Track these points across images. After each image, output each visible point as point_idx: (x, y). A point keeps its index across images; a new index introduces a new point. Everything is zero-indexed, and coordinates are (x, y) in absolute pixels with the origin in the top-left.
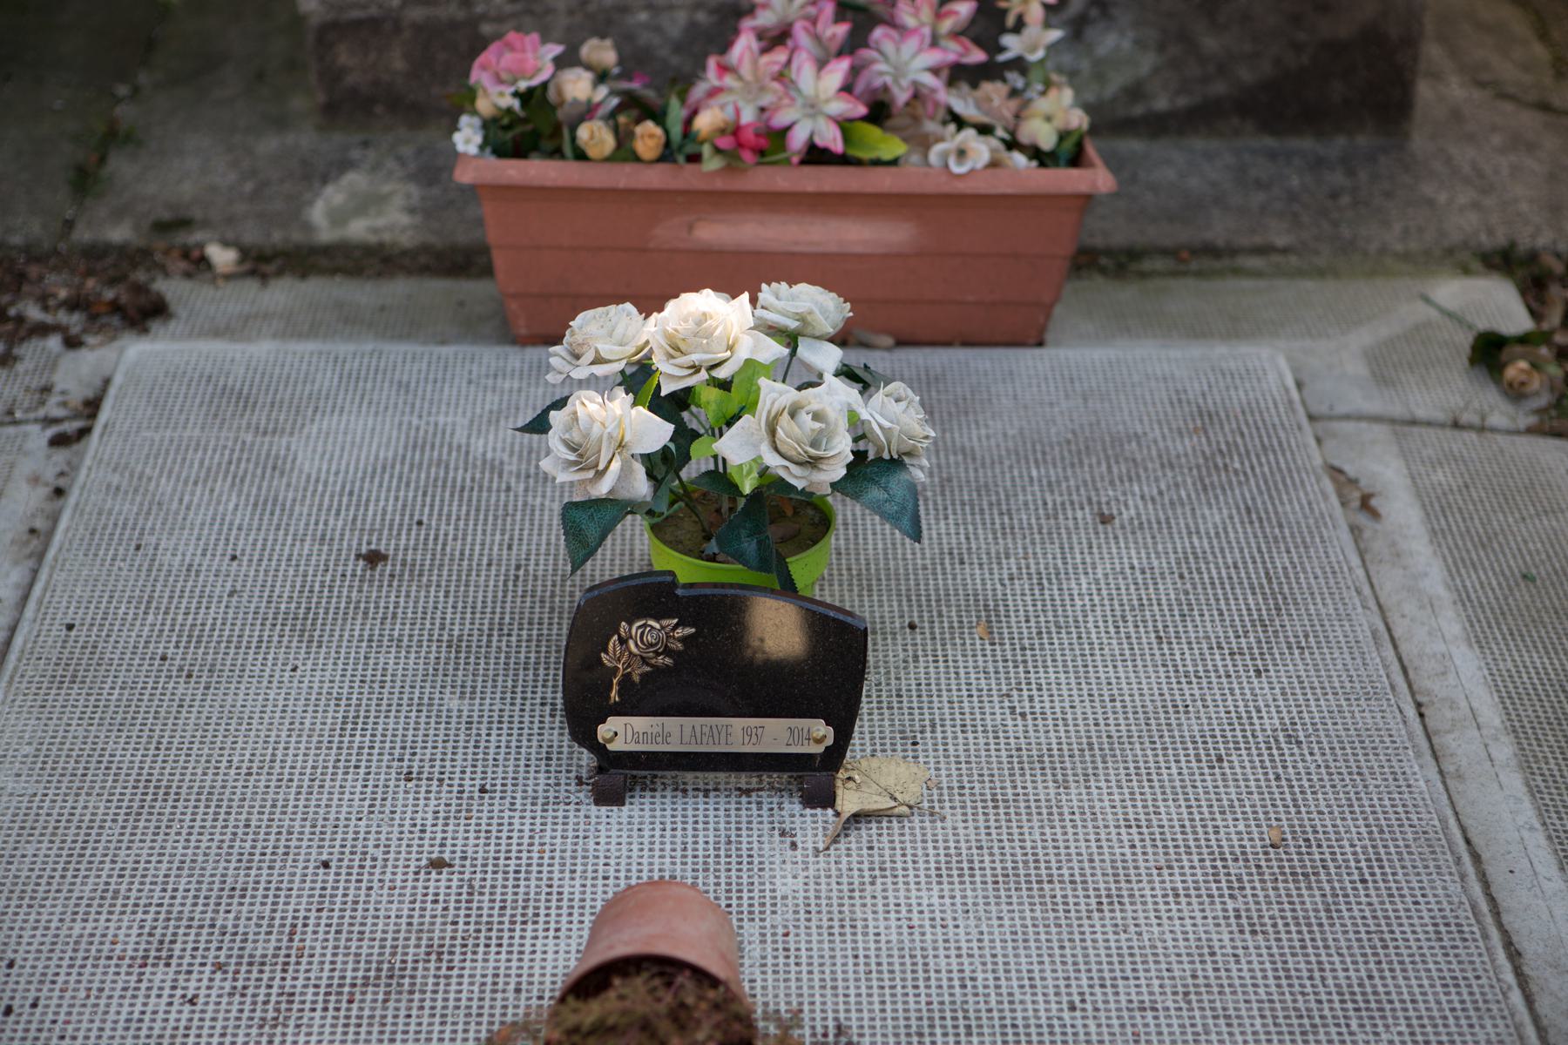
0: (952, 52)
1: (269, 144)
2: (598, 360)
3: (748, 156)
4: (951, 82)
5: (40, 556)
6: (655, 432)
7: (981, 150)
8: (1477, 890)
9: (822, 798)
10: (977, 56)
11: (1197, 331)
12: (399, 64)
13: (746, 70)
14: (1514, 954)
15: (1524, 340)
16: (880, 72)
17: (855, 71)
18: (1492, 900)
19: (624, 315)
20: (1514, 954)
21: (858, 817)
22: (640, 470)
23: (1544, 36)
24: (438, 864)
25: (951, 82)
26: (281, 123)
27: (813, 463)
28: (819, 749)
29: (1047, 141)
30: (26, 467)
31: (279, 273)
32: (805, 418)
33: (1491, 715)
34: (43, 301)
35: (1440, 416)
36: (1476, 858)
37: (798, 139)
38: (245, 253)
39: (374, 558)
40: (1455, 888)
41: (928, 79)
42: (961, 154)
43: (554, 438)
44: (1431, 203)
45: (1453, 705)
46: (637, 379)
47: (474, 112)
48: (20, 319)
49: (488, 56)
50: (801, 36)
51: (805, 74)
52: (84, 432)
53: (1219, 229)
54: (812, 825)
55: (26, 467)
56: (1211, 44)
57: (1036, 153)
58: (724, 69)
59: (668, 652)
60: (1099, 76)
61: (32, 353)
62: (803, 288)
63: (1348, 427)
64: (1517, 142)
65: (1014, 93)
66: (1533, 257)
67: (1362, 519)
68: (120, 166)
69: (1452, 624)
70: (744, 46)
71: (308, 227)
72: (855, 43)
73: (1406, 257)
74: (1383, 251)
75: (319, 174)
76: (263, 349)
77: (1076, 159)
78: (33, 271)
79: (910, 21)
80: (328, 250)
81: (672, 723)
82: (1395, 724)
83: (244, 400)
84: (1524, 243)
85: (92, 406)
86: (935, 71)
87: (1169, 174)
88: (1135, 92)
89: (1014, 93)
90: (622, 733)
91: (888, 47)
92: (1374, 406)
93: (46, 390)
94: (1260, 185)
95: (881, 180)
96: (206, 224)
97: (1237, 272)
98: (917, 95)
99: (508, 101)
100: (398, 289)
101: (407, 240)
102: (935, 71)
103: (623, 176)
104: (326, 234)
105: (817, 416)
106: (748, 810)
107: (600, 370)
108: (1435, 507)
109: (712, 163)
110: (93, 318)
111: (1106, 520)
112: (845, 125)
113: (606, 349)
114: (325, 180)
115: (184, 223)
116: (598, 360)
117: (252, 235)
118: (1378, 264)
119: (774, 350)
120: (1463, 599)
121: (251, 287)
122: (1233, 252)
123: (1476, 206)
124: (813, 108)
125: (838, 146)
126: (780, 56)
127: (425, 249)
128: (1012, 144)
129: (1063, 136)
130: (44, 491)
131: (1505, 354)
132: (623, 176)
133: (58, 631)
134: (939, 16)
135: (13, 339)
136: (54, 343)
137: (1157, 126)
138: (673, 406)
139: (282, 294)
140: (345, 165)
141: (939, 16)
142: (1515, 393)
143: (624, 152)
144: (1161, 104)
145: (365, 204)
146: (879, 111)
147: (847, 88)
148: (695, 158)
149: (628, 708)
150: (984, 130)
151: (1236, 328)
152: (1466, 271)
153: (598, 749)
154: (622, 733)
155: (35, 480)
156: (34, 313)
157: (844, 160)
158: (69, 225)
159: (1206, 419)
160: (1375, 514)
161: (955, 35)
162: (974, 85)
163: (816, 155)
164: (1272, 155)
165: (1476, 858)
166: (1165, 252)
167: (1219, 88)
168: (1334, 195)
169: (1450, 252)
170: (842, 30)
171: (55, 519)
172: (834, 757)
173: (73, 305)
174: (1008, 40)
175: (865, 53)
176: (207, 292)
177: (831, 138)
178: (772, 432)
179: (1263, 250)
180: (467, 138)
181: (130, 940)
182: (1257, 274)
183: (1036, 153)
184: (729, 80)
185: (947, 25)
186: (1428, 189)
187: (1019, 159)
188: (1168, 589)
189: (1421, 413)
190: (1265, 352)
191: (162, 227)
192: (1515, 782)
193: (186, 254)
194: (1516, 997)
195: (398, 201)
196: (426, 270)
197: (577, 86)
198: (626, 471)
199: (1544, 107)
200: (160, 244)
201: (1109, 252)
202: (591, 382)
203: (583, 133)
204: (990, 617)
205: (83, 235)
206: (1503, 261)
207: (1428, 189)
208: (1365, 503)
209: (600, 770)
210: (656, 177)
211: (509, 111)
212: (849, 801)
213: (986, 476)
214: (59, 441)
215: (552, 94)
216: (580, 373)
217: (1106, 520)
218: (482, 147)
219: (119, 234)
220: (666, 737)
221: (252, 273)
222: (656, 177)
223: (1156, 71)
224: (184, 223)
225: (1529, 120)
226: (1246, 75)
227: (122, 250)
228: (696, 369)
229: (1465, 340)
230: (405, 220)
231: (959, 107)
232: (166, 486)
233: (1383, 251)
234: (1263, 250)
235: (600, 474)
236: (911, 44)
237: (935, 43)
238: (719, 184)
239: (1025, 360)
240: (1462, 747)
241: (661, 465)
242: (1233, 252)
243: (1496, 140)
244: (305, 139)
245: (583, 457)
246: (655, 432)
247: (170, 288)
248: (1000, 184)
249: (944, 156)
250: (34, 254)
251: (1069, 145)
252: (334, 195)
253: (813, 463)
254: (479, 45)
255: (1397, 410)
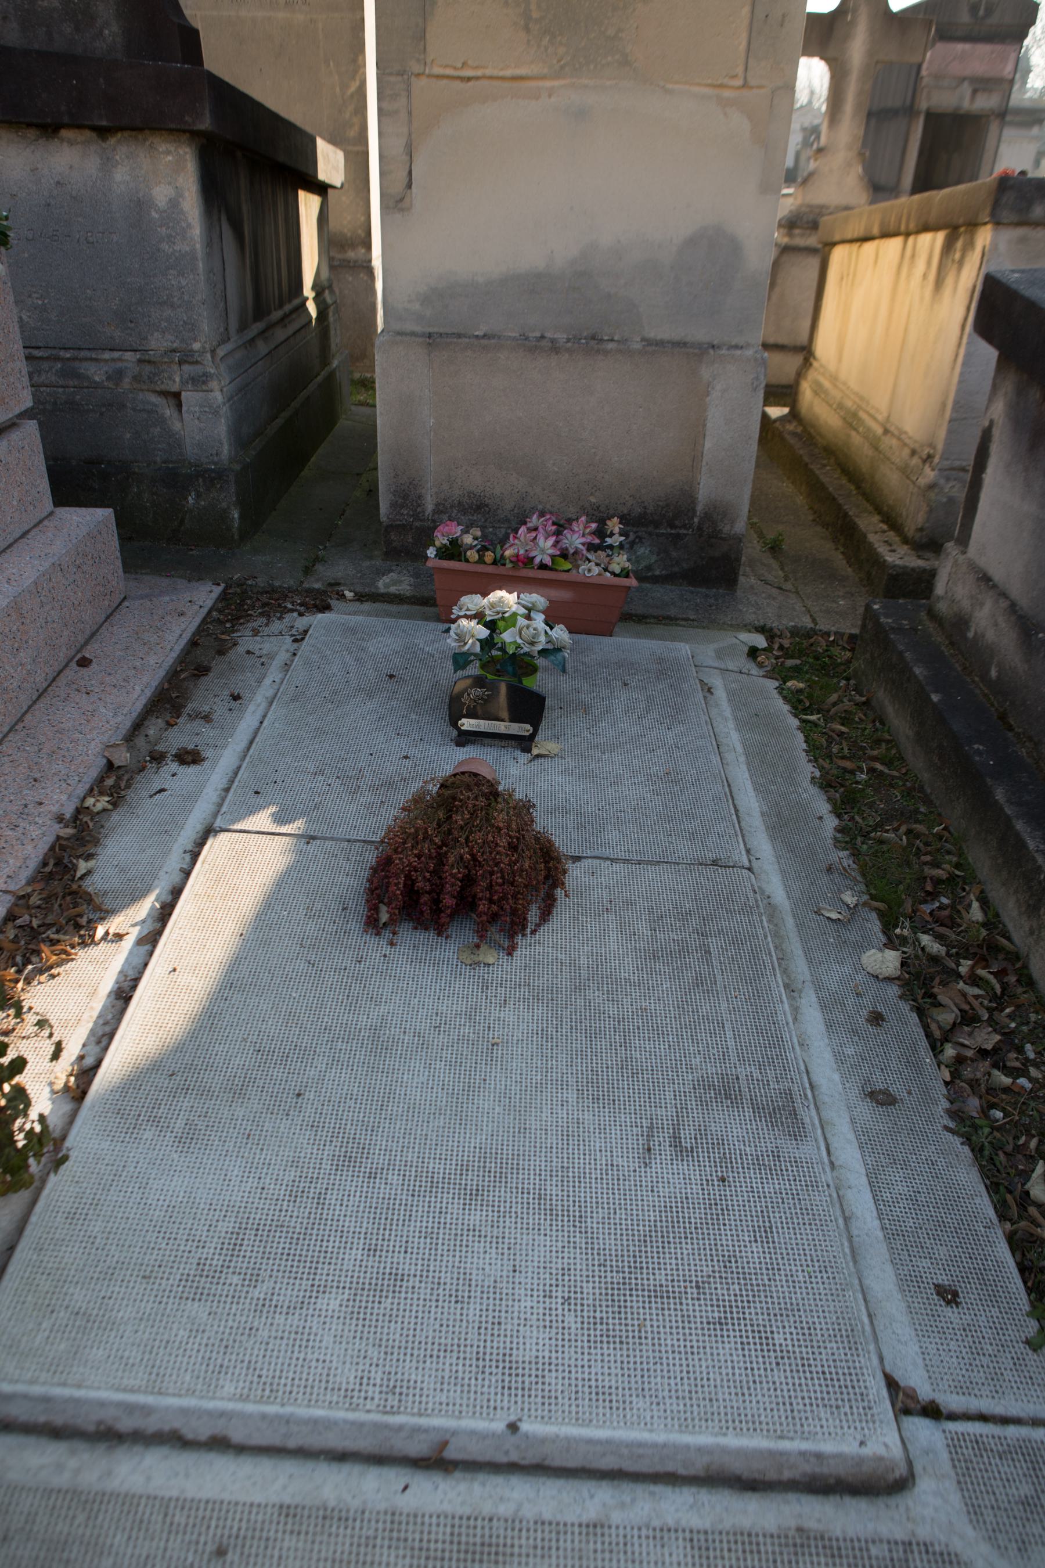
0: (588, 539)
1: (367, 563)
2: (468, 610)
3: (520, 564)
4: (588, 550)
5: (287, 671)
6: (483, 632)
7: (596, 570)
8: (727, 790)
9: (528, 750)
10: (597, 541)
11: (662, 638)
12: (410, 540)
13: (522, 538)
14: (737, 811)
15: (764, 650)
16: (565, 542)
17: (557, 542)
18: (731, 792)
19: (477, 598)
20: (737, 811)
21: (538, 756)
22: (478, 644)
23: (782, 569)
24: (406, 757)
25: (588, 550)
26: (371, 558)
27: (532, 644)
28: (527, 734)
29: (617, 570)
30: (285, 647)
31: (367, 601)
32: (531, 629)
33: (740, 749)
34: (293, 603)
35: (736, 669)
36: (729, 786)
37: (537, 560)
38: (356, 594)
39: (391, 676)
40: (720, 788)
41: (580, 546)
42: (589, 571)
43: (452, 633)
44: (741, 611)
45: (728, 746)
46: (479, 616)
47: (434, 546)
48: (285, 607)
49: (440, 528)
50: (540, 529)
51: (541, 541)
52: (303, 639)
53: (673, 612)
54: (523, 758)
55: (285, 647)
56: (674, 554)
57: (613, 574)
58: (515, 538)
59: (482, 699)
60: (638, 562)
61: (288, 617)
62: (534, 595)
63: (707, 669)
64: (770, 597)
65: (608, 556)
66: (771, 629)
67: (708, 695)
68: (319, 567)
69: (731, 725)
70: (522, 530)
71: (377, 587)
72: (558, 533)
73: (731, 625)
74: (724, 623)
75: (382, 573)
76: (360, 618)
77: (627, 576)
78: (290, 595)
79: (576, 529)
80: (382, 595)
81: (482, 722)
82: (708, 745)
83: (354, 631)
84: (769, 625)
85: (306, 632)
86: (583, 544)
87: (659, 595)
88: (649, 568)
89: (608, 556)
90: (468, 724)
91: (569, 536)
92: (716, 665)
93: (292, 627)
94: (686, 600)
95: (564, 577)
96: (345, 585)
97: (676, 625)
98: (576, 552)
99: (445, 541)
100: (405, 608)
101: (408, 594)
102: (583, 544)
103: (480, 568)
104: (382, 590)
105: (535, 629)
106: (504, 752)
107: (468, 613)
108: (732, 695)
109: (509, 565)
110: (308, 608)
111: (626, 685)
112: (553, 557)
113: (470, 606)
114: (383, 575)
115: (339, 584)
116: (468, 610)
117: (359, 589)
118: (722, 627)
119: (523, 611)
120: (736, 718)
121: (358, 604)
122: (677, 619)
123: (755, 613)
124: (543, 551)
125: (550, 564)
126: (534, 534)
127: (413, 597)
128: (606, 570)
129: (623, 569)
130: (290, 654)
131: (758, 653)
132: (480, 568)
133: (293, 688)
134: (586, 528)
135: (282, 613)
136: (295, 614)
137: (655, 580)
138: (491, 625)
139: (367, 606)
140: (391, 571)
141: (586, 528)
142: (760, 665)
143: (481, 561)
144: (657, 573)
145: (395, 583)
146: (564, 555)
147: (554, 546)
148: (504, 565)
149: (469, 716)
150: (597, 565)
151: (674, 639)
152: (750, 632)
153: (458, 729)
154: (468, 724)
155: (287, 651)
156: (290, 606)
157: (551, 569)
158: (302, 582)
159: (661, 660)
160: (712, 693)
161: (590, 534)
162: (595, 552)
163: (543, 567)
164: (692, 593)
165: (729, 786)
166: (655, 617)
167: (676, 569)
168: (710, 606)
169: (745, 626)
170: (554, 528)
171: (292, 661)
172: (532, 737)
173: (301, 605)
174: (607, 539)
175: (561, 537)
176: (344, 604)
177: (547, 560)
178: (520, 633)
179: (686, 619)
180: (431, 552)
181: (312, 768)
182: (681, 626)
183: (613, 574)
184: (516, 541)
185: (588, 530)
186: (740, 607)
187: (608, 574)
188: (643, 705)
189: (730, 668)
190: (682, 644)
191: (330, 585)
192: (744, 767)
193: (338, 594)
194: (734, 817)
195: (406, 582)
196: (413, 603)
197: (468, 539)
198: (473, 644)
199: (780, 588)
200: (330, 589)
201: (636, 616)
202: (466, 617)
203: (468, 553)
204: (586, 708)
205: (306, 585)
206: (761, 630)
207: (740, 607)
208: (709, 690)
209: (459, 736)
210: (491, 569)
211: (445, 545)
212: (535, 752)
213: (753, 1560)
214: (295, 641)
215: (459, 542)
216: (462, 613)
217: (626, 685)
218: (436, 556)
219: (317, 586)
220: (480, 726)
221: (358, 600)
222: (491, 569)
223: (656, 561)
224: (339, 584)
225: (775, 592)
226: (685, 566)
227: (318, 590)
228: (498, 613)
229: (746, 649)
230: (408, 588)
231: (590, 557)
232: (328, 652)
233: (724, 623)
234: (686, 619)
235: (465, 644)
236: (576, 536)
237: (583, 536)
238: (511, 573)
239: (606, 640)
240: (729, 757)
241: (487, 644)
242: (677, 619)
243: (764, 595)
244: (378, 563)
245: (461, 638)
246: (483, 632)
247: (333, 603)
248: (601, 581)
249: (584, 570)
250: (290, 589)
251: (624, 572)
252: (386, 579)
253: (532, 644)
254: (435, 528)
255: (723, 666)
